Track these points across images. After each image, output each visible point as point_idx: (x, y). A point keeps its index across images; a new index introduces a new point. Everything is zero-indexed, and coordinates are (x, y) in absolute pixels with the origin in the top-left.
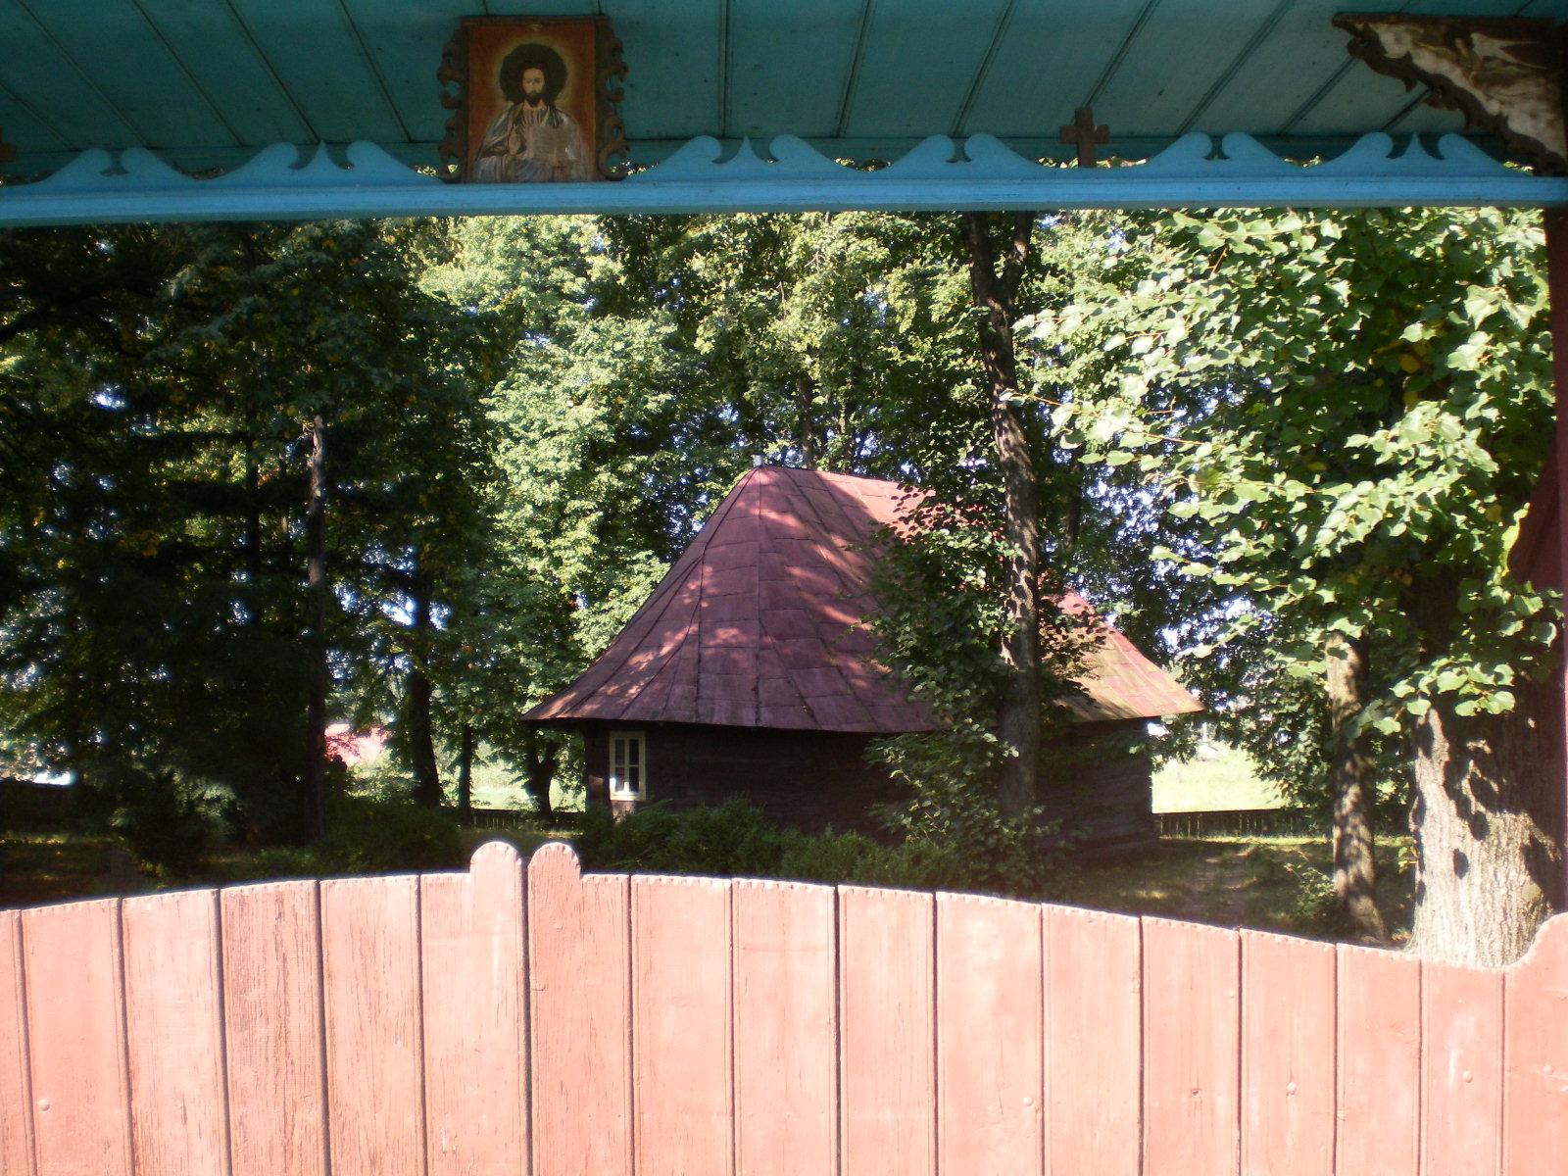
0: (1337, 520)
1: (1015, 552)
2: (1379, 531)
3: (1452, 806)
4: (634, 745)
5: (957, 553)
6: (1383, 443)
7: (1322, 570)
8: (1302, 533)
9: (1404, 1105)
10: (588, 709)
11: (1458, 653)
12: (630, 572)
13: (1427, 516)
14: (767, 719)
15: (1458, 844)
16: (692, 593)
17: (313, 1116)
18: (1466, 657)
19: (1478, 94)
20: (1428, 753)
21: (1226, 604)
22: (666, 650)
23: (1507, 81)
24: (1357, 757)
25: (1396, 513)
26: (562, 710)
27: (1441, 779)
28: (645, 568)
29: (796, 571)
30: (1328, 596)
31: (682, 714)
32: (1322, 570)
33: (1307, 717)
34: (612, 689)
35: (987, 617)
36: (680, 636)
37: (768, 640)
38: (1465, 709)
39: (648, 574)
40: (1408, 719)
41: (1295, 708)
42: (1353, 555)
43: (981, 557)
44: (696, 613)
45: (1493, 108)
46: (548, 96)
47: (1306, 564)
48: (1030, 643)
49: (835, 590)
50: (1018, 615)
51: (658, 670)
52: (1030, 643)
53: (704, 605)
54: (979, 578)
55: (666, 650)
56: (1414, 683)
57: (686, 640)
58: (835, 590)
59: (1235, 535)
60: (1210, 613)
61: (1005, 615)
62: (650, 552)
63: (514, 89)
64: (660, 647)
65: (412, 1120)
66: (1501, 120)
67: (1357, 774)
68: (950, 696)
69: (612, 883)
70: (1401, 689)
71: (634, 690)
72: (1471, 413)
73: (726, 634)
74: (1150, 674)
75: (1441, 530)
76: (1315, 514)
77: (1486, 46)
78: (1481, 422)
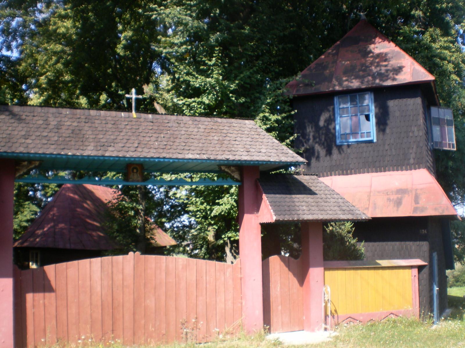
0: (214, 212)
1: (141, 207)
2: (220, 214)
3: (231, 254)
4: (37, 254)
5: (126, 208)
6: (220, 201)
7: (212, 218)
8: (209, 212)
9: (223, 278)
10: (26, 244)
11: (231, 231)
12: (24, 208)
13: (227, 211)
14: (73, 247)
15: (232, 260)
16: (51, 215)
17: (111, 282)
18: (232, 232)
19: (231, 173)
20: (227, 246)
21: (181, 217)
22: (46, 229)
23: (234, 172)
24: (215, 254)
25: (223, 211)
26: (18, 244)
27: (229, 250)
28: (28, 206)
29: (78, 210)
30: (213, 222)
31: (51, 245)
32: (212, 218)
33: (204, 245)
34: (32, 239)
35: (134, 222)
36: (49, 226)
37: (72, 227)
38: (232, 239)
39: (29, 208)
40: (224, 241)
41: (201, 243)
42: (215, 216)
43: (132, 209)
44: (52, 220)
45: (233, 175)
46: (137, 172)
47: (209, 217)
48: (143, 229)
49: (88, 214)
50: (141, 221)
51: (44, 234)
52: (143, 229)
53: (55, 218)
54: (132, 213)
55: (46, 229)
56: (225, 235)
57: (51, 227)
58: (88, 214)
59: (199, 213)
60: (177, 219)
61: (137, 222)
62: (29, 202)
63: (133, 172)
64: (44, 229)
65: (122, 282)
66: (233, 176)
67: (215, 258)
68: (125, 240)
69: (144, 256)
70: (223, 236)
71: (38, 240)
72: (233, 197)
73: (62, 225)
74: (164, 235)
75: (229, 213)
76: (211, 210)
77: (232, 168)
78: (234, 198)
